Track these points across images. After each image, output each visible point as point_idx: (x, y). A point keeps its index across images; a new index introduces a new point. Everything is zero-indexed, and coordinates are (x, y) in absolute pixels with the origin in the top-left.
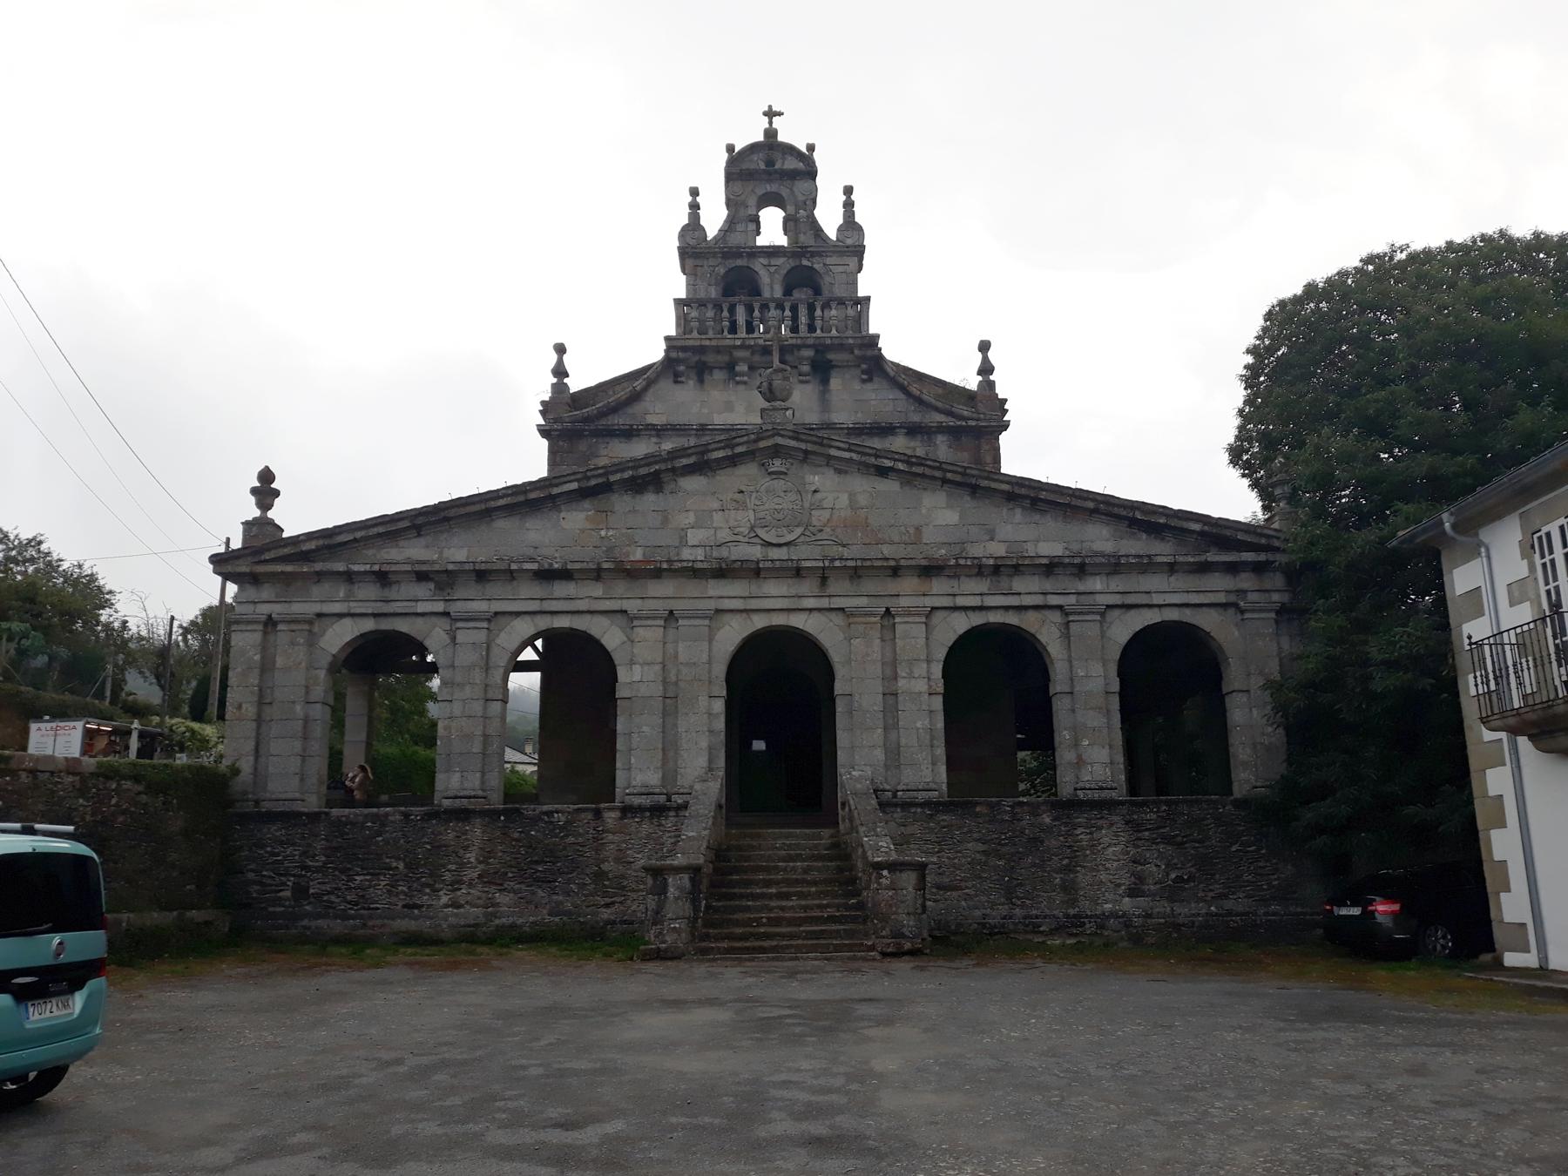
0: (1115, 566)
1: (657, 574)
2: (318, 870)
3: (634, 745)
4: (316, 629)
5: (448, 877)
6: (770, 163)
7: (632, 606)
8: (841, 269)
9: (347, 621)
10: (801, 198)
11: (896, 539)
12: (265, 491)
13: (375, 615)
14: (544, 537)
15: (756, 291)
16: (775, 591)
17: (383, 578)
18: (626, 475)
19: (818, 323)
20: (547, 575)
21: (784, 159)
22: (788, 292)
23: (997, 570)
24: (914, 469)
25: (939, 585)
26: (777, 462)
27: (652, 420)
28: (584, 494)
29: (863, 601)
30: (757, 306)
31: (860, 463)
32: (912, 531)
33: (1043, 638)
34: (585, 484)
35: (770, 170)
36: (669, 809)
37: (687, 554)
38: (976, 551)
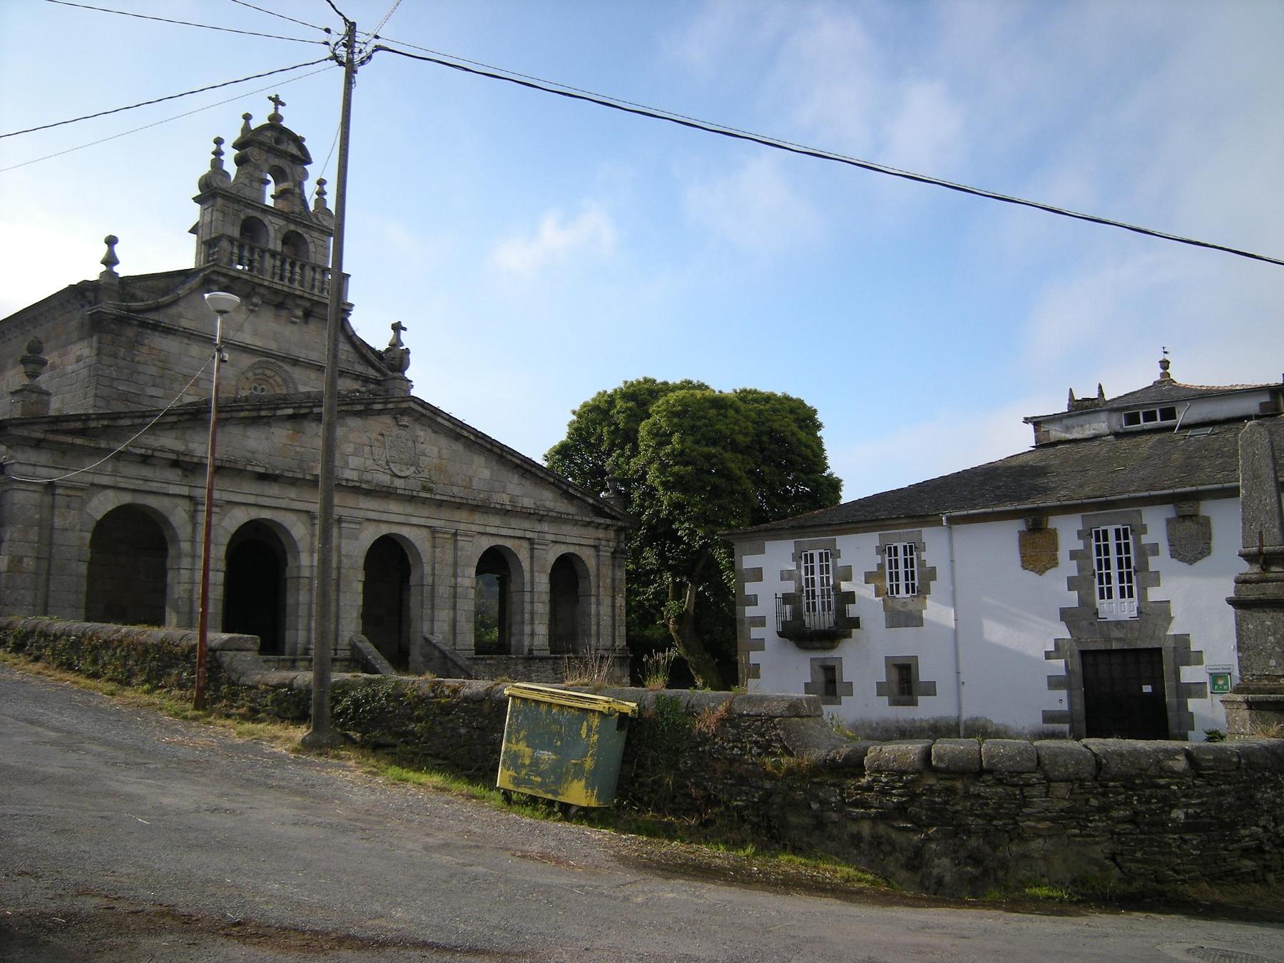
9: (110, 493)
13: (134, 491)
16: (395, 509)
20: (263, 477)
23: (504, 512)
26: (406, 419)
27: (185, 323)
29: (441, 523)
31: (451, 430)
33: (520, 557)
35: (272, 147)
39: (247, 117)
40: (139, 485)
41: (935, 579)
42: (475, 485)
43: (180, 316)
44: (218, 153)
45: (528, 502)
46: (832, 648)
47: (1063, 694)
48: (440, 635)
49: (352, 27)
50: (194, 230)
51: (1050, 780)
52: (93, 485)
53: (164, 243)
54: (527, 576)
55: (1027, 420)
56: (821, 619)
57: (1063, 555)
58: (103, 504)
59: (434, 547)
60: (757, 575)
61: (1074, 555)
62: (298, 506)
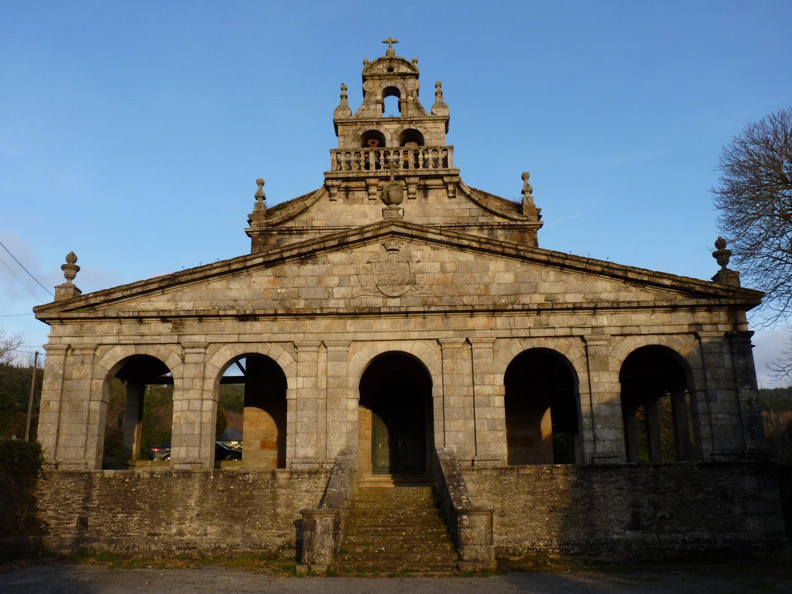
0: (615, 307)
1: (312, 316)
2: (94, 509)
3: (299, 430)
4: (98, 353)
5: (177, 515)
6: (390, 69)
7: (298, 338)
8: (435, 130)
10: (410, 89)
11: (472, 292)
12: (71, 266)
14: (238, 291)
15: (382, 143)
17: (140, 319)
18: (295, 252)
19: (421, 162)
20: (243, 318)
21: (399, 67)
22: (402, 145)
24: (483, 246)
25: (500, 321)
28: (268, 264)
30: (382, 152)
32: (482, 287)
34: (267, 259)
36: (321, 473)
37: (332, 303)
38: (526, 300)
40: (138, 339)
42: (494, 290)
43: (313, 219)
46: (690, 369)
51: (203, 390)
62: (283, 337)
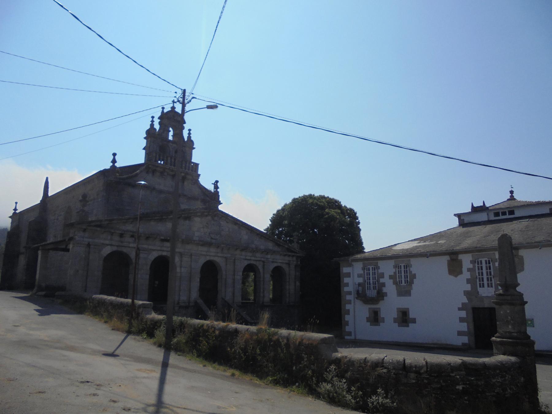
9: (109, 247)
13: (117, 246)
33: (259, 268)
35: (173, 119)
39: (163, 108)
41: (415, 278)
44: (153, 121)
45: (262, 247)
47: (465, 324)
48: (228, 298)
49: (184, 92)
50: (144, 149)
52: (103, 244)
53: (134, 154)
54: (262, 274)
55: (455, 215)
56: (372, 293)
57: (464, 269)
58: (107, 251)
59: (226, 265)
60: (348, 275)
61: (469, 270)
